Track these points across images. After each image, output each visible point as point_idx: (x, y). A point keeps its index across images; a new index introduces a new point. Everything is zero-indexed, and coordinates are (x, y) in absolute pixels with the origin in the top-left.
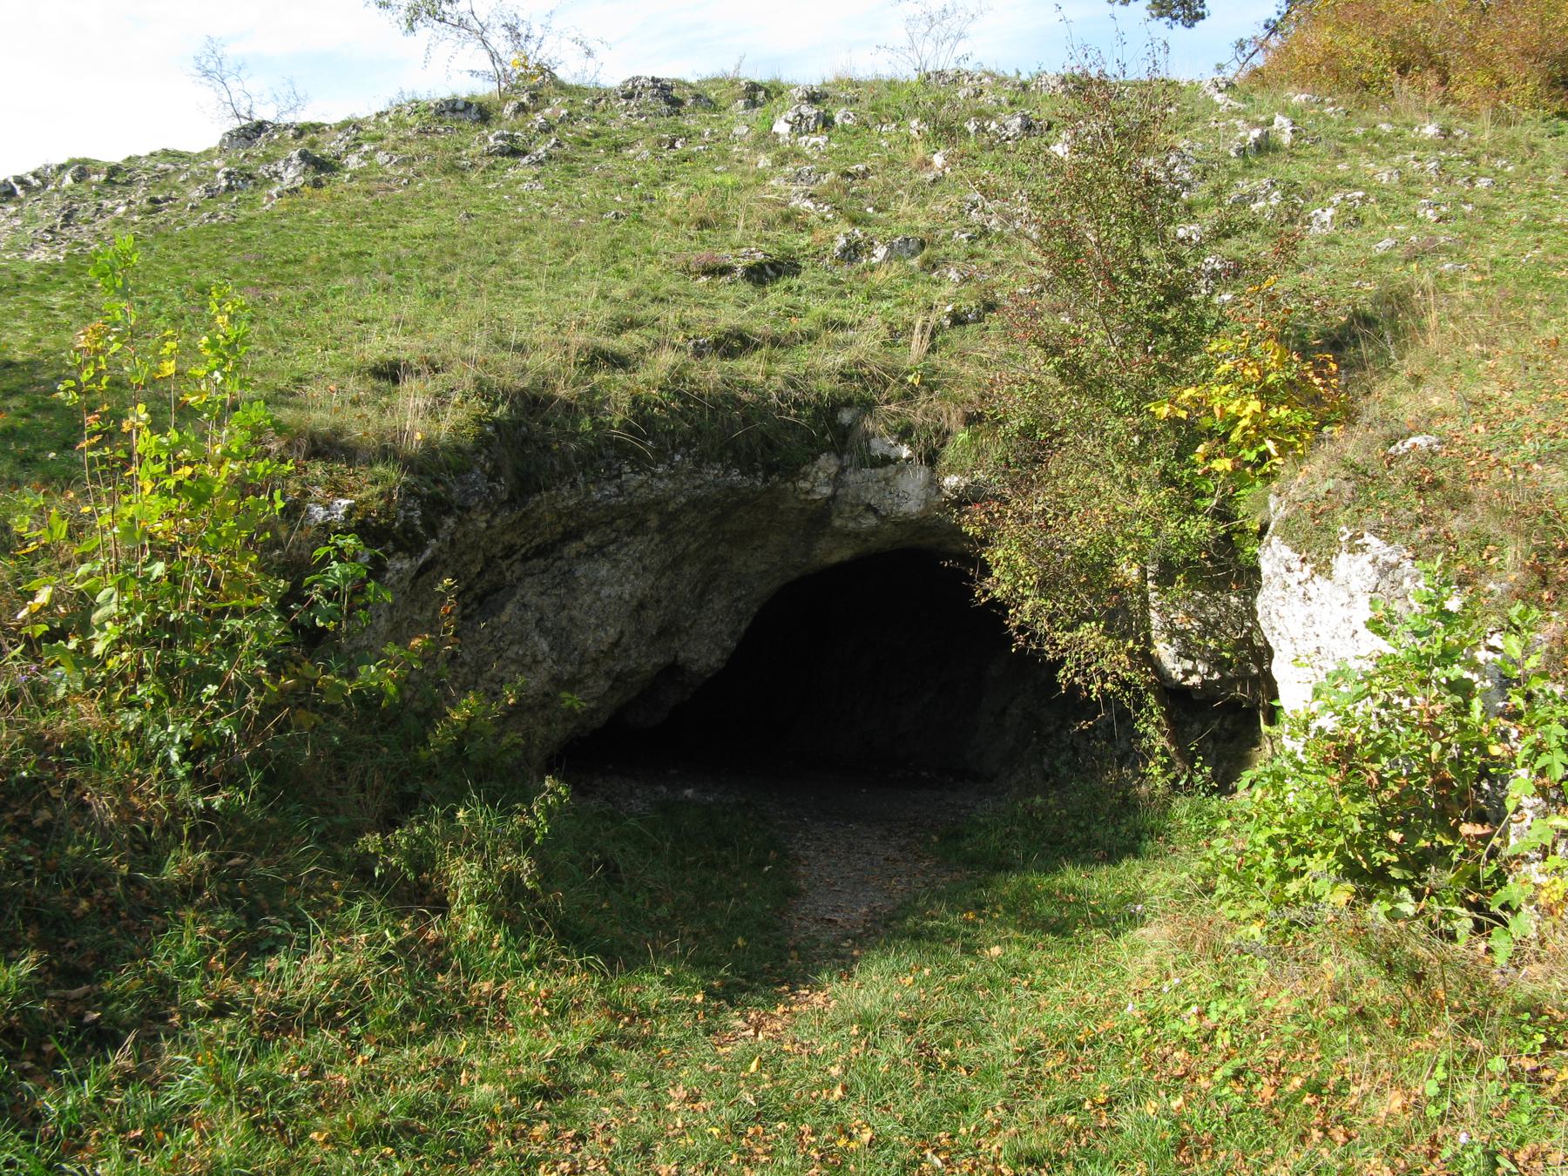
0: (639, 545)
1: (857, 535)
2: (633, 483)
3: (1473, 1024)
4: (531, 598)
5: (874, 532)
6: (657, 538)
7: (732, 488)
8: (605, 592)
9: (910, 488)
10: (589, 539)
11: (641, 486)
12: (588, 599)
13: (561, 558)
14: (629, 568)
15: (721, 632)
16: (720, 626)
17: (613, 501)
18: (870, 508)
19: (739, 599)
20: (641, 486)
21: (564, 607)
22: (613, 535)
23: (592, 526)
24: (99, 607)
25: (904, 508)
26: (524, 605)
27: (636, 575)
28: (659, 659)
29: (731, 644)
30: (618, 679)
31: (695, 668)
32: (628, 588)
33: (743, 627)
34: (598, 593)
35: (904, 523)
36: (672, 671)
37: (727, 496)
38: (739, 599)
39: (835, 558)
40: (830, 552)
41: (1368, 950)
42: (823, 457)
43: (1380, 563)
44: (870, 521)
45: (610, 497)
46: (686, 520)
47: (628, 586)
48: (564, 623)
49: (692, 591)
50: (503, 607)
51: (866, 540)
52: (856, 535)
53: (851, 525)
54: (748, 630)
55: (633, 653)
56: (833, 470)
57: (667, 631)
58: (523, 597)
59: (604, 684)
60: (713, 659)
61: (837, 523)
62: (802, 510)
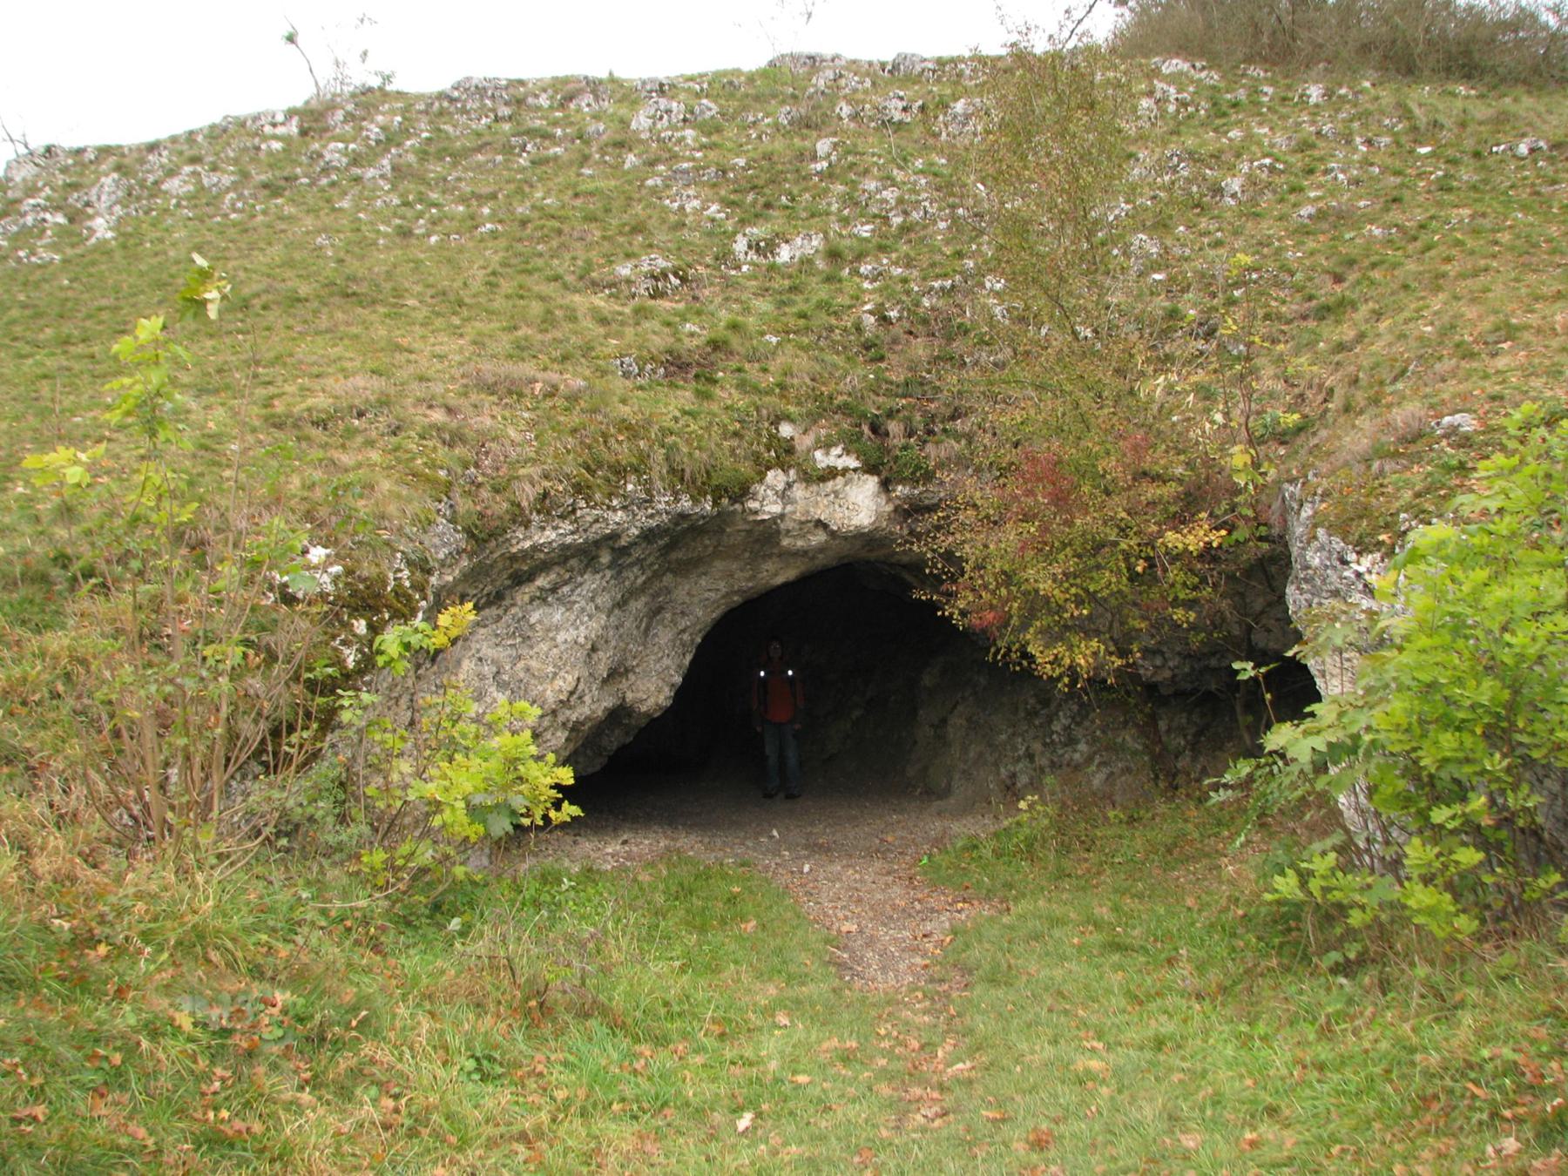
0: (591, 582)
1: (805, 553)
2: (589, 519)
3: (1470, 1066)
4: (487, 651)
5: (822, 549)
6: (609, 574)
7: (683, 516)
8: (561, 637)
9: (860, 499)
10: (542, 582)
11: (597, 521)
12: (544, 647)
13: (513, 605)
14: (583, 610)
15: (668, 668)
16: (666, 662)
17: (569, 540)
18: (820, 524)
19: (683, 631)
20: (597, 521)
21: (519, 657)
22: (567, 576)
23: (544, 567)
24: (1334, 848)
25: (856, 521)
26: (480, 659)
27: (590, 617)
28: (609, 702)
29: (678, 679)
30: (575, 728)
31: (644, 709)
32: (583, 630)
33: (689, 658)
34: (553, 639)
35: (854, 537)
36: (619, 714)
37: (677, 524)
38: (683, 631)
39: (780, 580)
40: (776, 575)
41: (1417, 778)
42: (770, 474)
43: (1288, 81)
44: (819, 538)
45: (565, 535)
46: (637, 553)
47: (582, 628)
48: (522, 675)
49: (638, 627)
50: (459, 663)
51: (813, 558)
52: (804, 553)
53: (800, 543)
54: (692, 662)
55: (587, 699)
56: (780, 487)
57: (616, 673)
58: (478, 651)
59: (562, 736)
60: (662, 697)
61: (785, 542)
62: (749, 532)
